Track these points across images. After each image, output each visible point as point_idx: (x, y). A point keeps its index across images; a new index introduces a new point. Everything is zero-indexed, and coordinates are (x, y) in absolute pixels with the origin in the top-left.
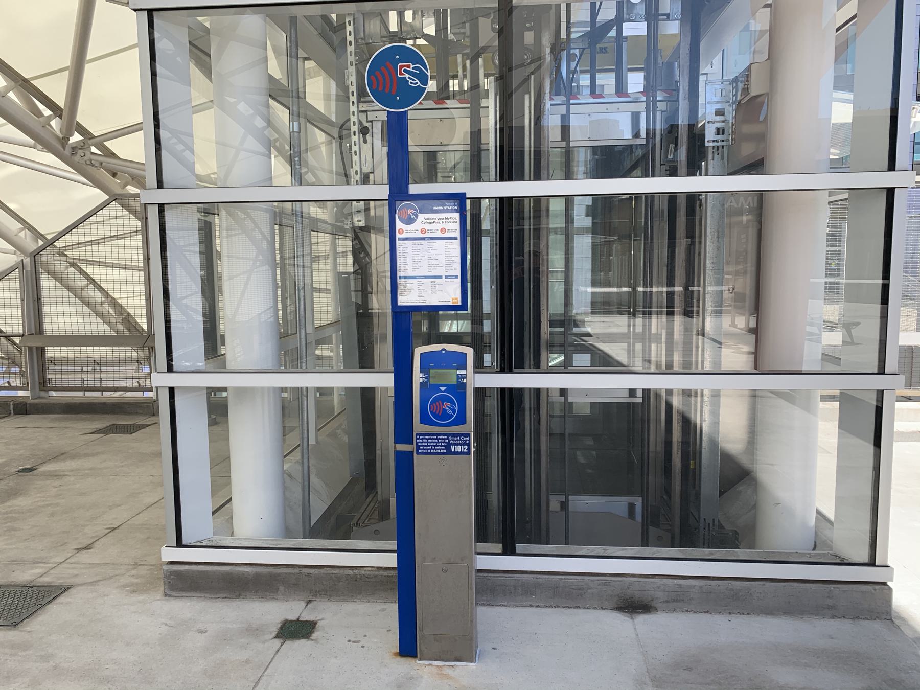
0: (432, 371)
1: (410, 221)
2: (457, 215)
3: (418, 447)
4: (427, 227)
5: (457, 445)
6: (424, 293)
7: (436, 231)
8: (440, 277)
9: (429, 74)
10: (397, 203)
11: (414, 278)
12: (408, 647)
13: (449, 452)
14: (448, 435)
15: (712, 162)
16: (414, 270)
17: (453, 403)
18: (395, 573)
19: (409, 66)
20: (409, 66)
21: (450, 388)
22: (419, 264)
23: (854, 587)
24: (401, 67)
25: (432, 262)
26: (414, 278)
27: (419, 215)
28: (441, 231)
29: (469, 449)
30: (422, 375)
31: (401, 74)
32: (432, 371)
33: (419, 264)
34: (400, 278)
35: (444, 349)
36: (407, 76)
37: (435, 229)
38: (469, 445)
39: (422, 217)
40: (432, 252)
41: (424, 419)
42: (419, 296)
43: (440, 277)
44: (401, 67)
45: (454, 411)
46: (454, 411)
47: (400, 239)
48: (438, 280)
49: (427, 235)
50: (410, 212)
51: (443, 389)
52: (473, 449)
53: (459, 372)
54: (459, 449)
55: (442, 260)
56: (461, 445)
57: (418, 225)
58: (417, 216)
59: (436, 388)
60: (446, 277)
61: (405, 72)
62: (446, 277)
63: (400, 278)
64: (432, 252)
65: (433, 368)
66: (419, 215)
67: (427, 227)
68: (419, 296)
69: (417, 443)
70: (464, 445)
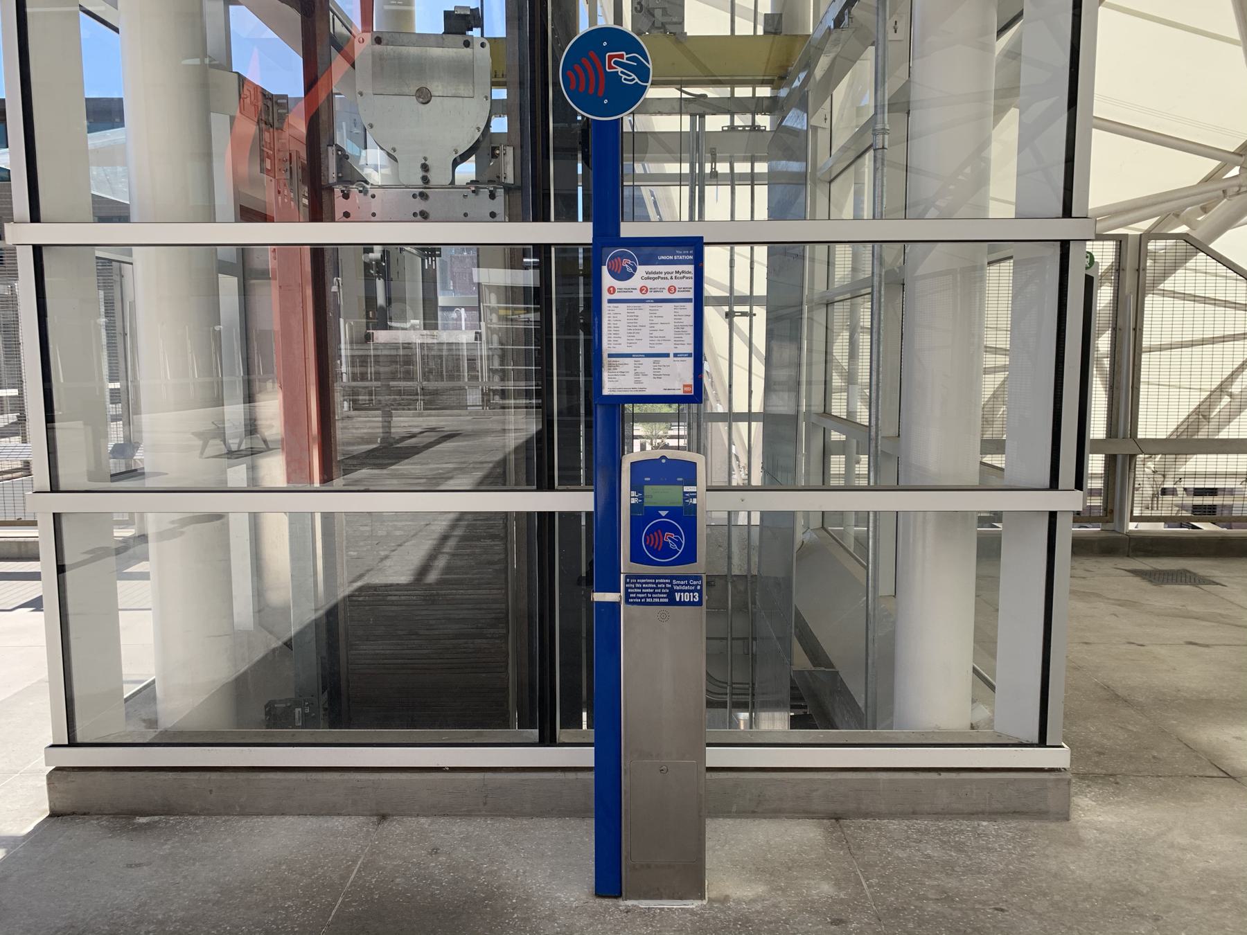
0: (647, 489)
1: (623, 275)
2: (691, 268)
3: (627, 594)
4: (650, 284)
5: (684, 591)
6: (642, 378)
7: (661, 290)
8: (667, 355)
9: (650, 66)
10: (605, 250)
11: (630, 356)
12: (609, 882)
13: (672, 602)
14: (672, 577)
15: (230, 255)
16: (630, 344)
17: (677, 532)
18: (591, 776)
19: (622, 57)
20: (622, 57)
21: (674, 512)
22: (637, 336)
23: (319, 776)
24: (611, 57)
25: (655, 334)
26: (630, 356)
27: (639, 268)
28: (641, 290)
29: (701, 597)
30: (634, 494)
31: (610, 67)
32: (647, 489)
33: (637, 336)
34: (690, 355)
35: (663, 457)
36: (620, 69)
37: (660, 287)
38: (700, 592)
39: (642, 270)
40: (656, 320)
41: (637, 556)
42: (636, 382)
43: (667, 355)
44: (611, 57)
45: (679, 544)
46: (679, 544)
47: (610, 301)
48: (663, 360)
49: (649, 296)
50: (626, 263)
51: (663, 513)
52: (705, 598)
53: (686, 489)
54: (686, 597)
55: (669, 331)
56: (689, 591)
57: (636, 281)
58: (635, 269)
59: (653, 512)
60: (676, 355)
61: (616, 64)
62: (676, 355)
63: (690, 355)
64: (656, 320)
65: (648, 483)
66: (639, 268)
67: (650, 284)
68: (636, 382)
69: (626, 589)
70: (695, 590)
